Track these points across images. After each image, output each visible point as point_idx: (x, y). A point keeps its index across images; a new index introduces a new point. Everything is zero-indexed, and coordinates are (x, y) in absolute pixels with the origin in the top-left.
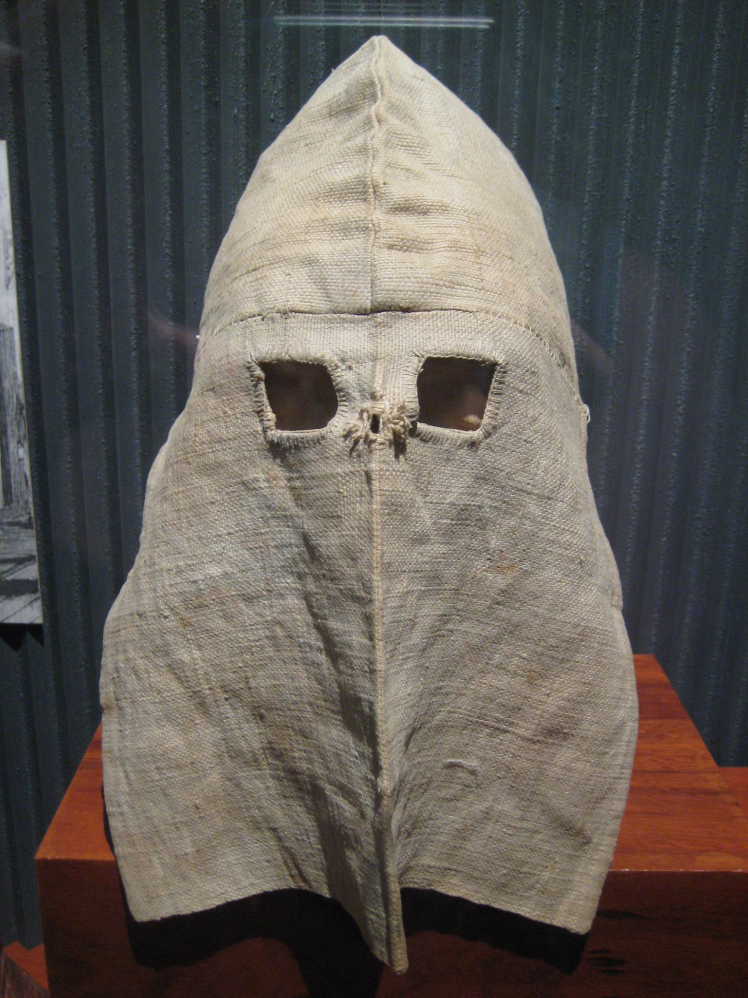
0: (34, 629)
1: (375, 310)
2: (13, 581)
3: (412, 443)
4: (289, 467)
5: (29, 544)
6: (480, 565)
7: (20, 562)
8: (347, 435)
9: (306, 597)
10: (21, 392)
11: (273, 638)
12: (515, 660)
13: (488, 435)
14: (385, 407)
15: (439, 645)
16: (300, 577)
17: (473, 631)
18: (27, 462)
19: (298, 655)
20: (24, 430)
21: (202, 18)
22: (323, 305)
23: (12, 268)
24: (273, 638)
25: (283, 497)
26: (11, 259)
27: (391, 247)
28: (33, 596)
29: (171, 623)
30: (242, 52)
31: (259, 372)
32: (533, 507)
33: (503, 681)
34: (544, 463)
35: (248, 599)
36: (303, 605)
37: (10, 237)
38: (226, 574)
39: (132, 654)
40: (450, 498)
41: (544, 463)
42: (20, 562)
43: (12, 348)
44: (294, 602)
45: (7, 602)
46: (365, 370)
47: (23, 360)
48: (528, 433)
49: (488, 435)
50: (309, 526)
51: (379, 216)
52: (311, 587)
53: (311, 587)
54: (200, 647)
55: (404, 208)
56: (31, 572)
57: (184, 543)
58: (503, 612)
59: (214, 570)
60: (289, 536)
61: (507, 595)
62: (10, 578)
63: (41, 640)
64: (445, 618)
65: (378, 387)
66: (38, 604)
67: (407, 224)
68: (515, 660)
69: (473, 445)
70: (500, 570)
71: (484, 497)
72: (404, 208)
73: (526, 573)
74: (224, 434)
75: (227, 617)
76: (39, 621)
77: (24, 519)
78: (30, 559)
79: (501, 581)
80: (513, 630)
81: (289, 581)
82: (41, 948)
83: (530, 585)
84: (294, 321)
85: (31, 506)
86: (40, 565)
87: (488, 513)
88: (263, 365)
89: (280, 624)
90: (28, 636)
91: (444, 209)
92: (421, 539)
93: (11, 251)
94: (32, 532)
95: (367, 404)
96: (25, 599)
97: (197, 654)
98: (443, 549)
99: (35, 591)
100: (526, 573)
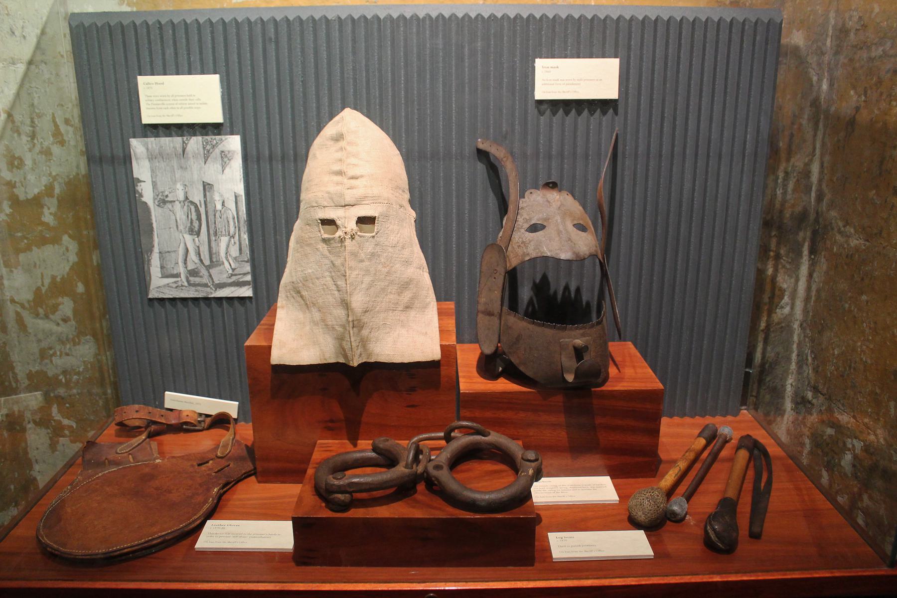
0: (250, 298)
1: (345, 206)
2: (243, 281)
3: (357, 237)
4: (327, 245)
5: (248, 268)
6: (380, 267)
7: (245, 274)
8: (340, 237)
9: (332, 277)
10: (245, 216)
11: (323, 289)
12: (394, 290)
13: (376, 234)
14: (348, 230)
15: (373, 289)
16: (330, 272)
17: (382, 284)
18: (247, 240)
19: (330, 293)
20: (246, 229)
21: (301, 95)
22: (333, 205)
23: (242, 175)
24: (323, 289)
25: (326, 253)
26: (242, 173)
27: (348, 189)
28: (249, 287)
29: (300, 285)
30: (314, 105)
31: (319, 221)
32: (390, 250)
33: (392, 296)
34: (392, 238)
35: (317, 279)
36: (331, 279)
37: (241, 165)
38: (313, 272)
39: (292, 293)
40: (369, 251)
41: (392, 238)
42: (245, 274)
43: (242, 201)
44: (328, 279)
45: (240, 289)
46: (343, 221)
47: (246, 205)
48: (387, 232)
49: (376, 234)
50: (333, 259)
51: (346, 181)
52: (333, 274)
53: (333, 274)
54: (307, 291)
55: (352, 178)
56: (249, 278)
57: (861, 346)
58: (388, 278)
59: (310, 271)
60: (327, 262)
61: (388, 273)
62: (241, 280)
63: (251, 302)
64: (373, 281)
65: (346, 225)
66: (251, 289)
67: (353, 182)
68: (394, 290)
69: (373, 237)
70: (385, 267)
71: (378, 249)
72: (352, 178)
73: (392, 267)
74: (312, 236)
75: (313, 284)
76: (251, 295)
77: (246, 259)
78: (248, 273)
79: (386, 270)
80: (392, 282)
81: (327, 273)
82: (251, 423)
83: (393, 269)
84: (326, 208)
85: (248, 255)
86: (252, 275)
87: (380, 253)
88: (321, 220)
89: (325, 285)
90: (247, 301)
91: (362, 176)
92: (362, 261)
93: (242, 170)
94: (249, 264)
95: (344, 229)
96: (246, 287)
97: (306, 293)
98: (369, 263)
99: (250, 285)
100: (392, 267)
